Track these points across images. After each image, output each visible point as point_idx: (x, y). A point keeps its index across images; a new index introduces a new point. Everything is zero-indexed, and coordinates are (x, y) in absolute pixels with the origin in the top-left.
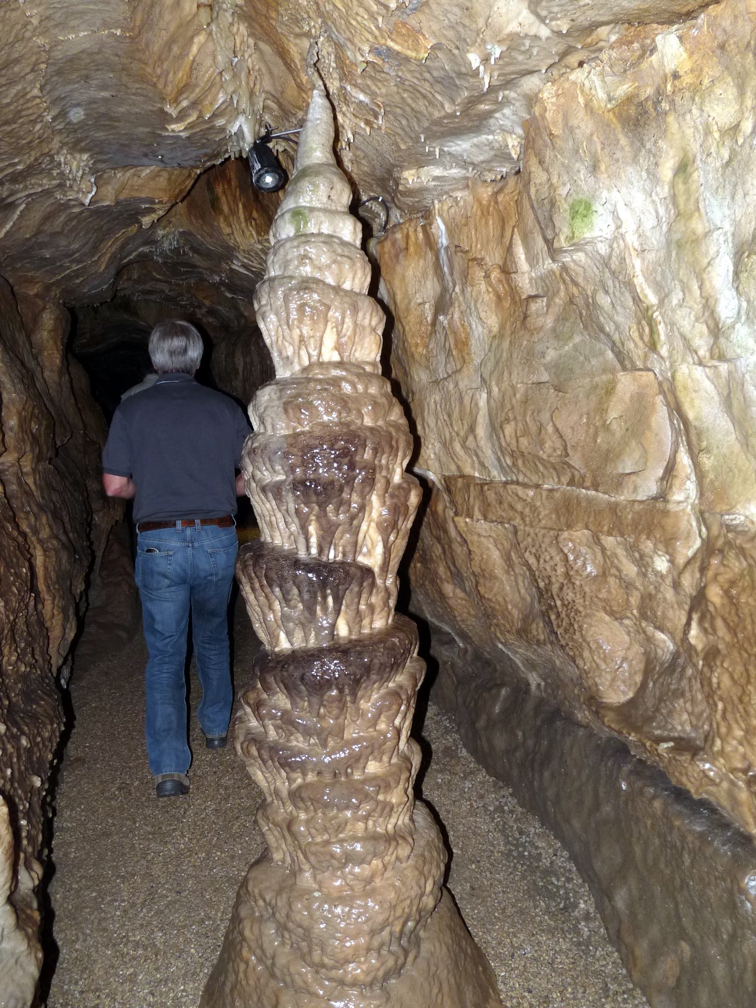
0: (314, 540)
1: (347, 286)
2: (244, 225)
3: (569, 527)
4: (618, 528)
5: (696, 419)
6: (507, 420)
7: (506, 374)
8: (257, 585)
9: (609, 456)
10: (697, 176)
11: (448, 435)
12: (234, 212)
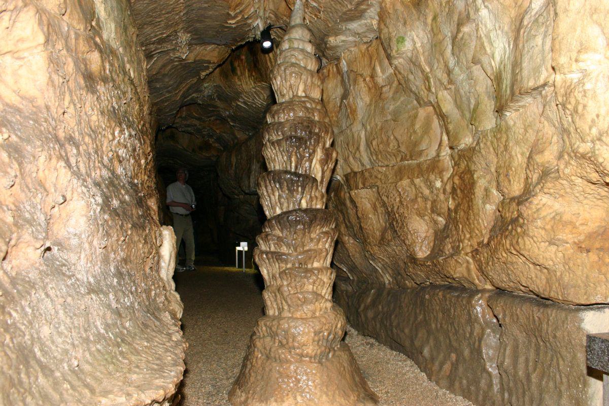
0: (293, 165)
1: (309, 68)
2: (248, 79)
3: (401, 179)
4: (421, 173)
5: (446, 112)
6: (374, 139)
7: (373, 119)
8: (268, 184)
9: (416, 144)
10: (439, 20)
11: (347, 154)
12: (242, 74)
